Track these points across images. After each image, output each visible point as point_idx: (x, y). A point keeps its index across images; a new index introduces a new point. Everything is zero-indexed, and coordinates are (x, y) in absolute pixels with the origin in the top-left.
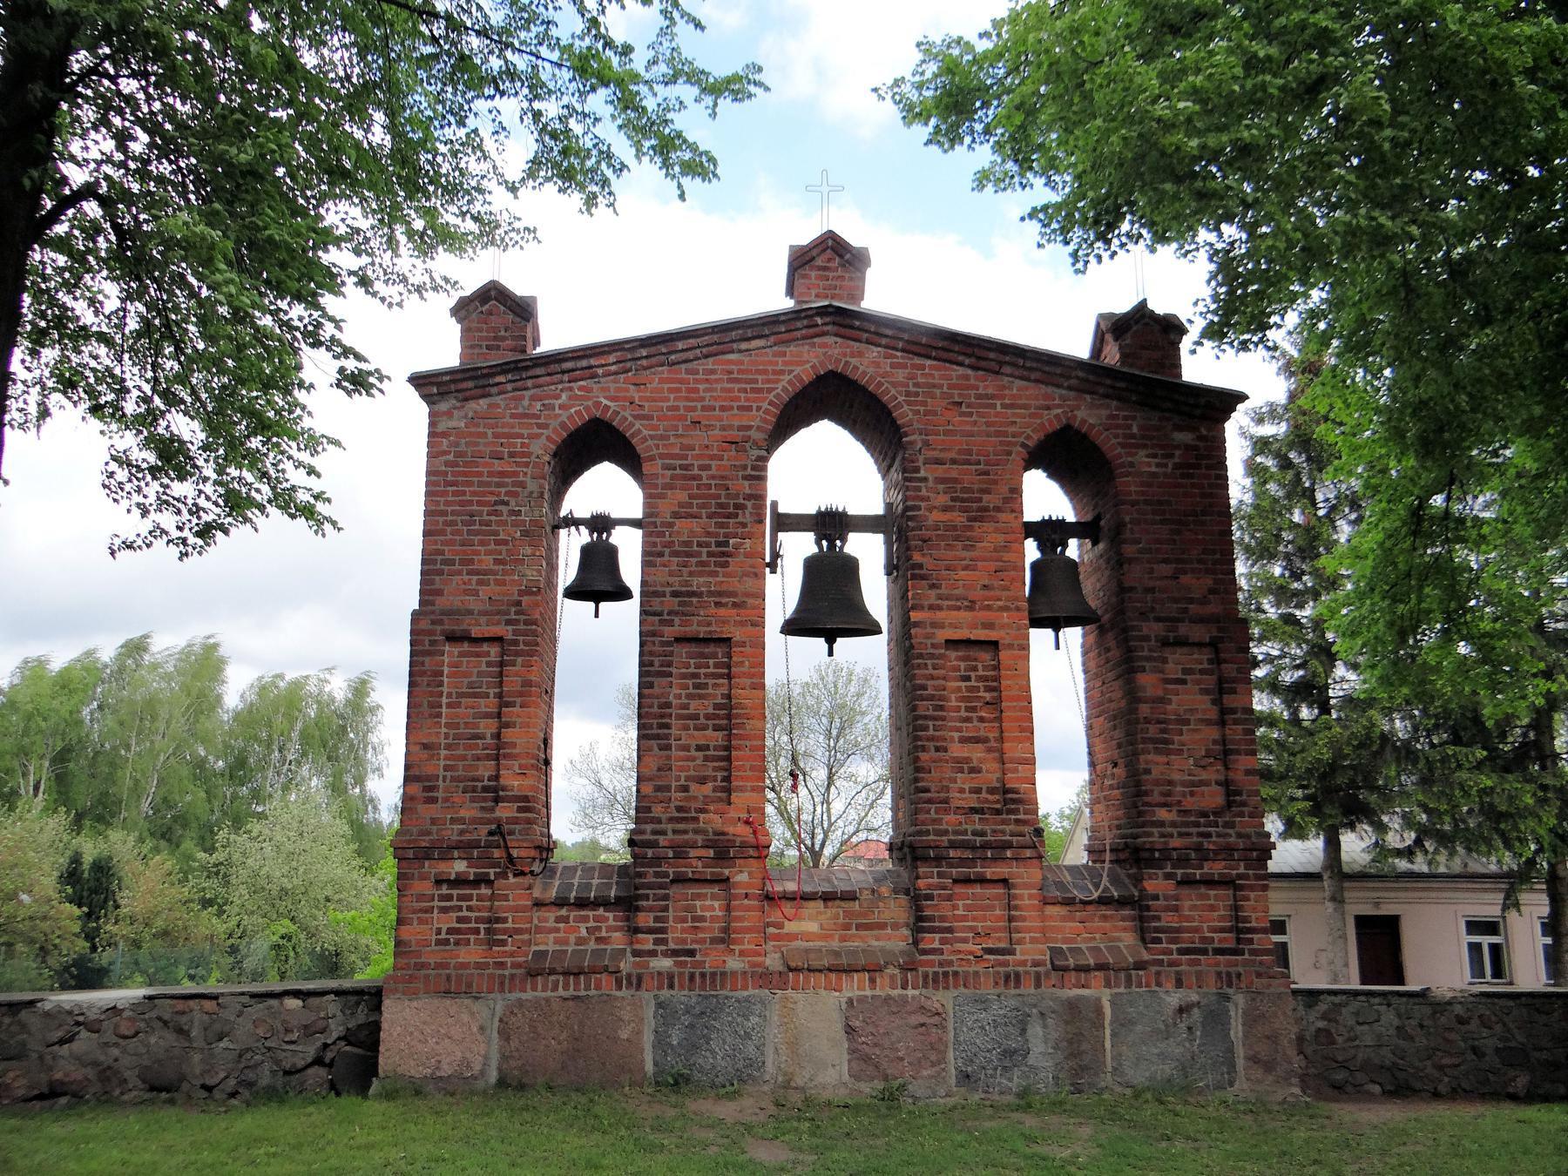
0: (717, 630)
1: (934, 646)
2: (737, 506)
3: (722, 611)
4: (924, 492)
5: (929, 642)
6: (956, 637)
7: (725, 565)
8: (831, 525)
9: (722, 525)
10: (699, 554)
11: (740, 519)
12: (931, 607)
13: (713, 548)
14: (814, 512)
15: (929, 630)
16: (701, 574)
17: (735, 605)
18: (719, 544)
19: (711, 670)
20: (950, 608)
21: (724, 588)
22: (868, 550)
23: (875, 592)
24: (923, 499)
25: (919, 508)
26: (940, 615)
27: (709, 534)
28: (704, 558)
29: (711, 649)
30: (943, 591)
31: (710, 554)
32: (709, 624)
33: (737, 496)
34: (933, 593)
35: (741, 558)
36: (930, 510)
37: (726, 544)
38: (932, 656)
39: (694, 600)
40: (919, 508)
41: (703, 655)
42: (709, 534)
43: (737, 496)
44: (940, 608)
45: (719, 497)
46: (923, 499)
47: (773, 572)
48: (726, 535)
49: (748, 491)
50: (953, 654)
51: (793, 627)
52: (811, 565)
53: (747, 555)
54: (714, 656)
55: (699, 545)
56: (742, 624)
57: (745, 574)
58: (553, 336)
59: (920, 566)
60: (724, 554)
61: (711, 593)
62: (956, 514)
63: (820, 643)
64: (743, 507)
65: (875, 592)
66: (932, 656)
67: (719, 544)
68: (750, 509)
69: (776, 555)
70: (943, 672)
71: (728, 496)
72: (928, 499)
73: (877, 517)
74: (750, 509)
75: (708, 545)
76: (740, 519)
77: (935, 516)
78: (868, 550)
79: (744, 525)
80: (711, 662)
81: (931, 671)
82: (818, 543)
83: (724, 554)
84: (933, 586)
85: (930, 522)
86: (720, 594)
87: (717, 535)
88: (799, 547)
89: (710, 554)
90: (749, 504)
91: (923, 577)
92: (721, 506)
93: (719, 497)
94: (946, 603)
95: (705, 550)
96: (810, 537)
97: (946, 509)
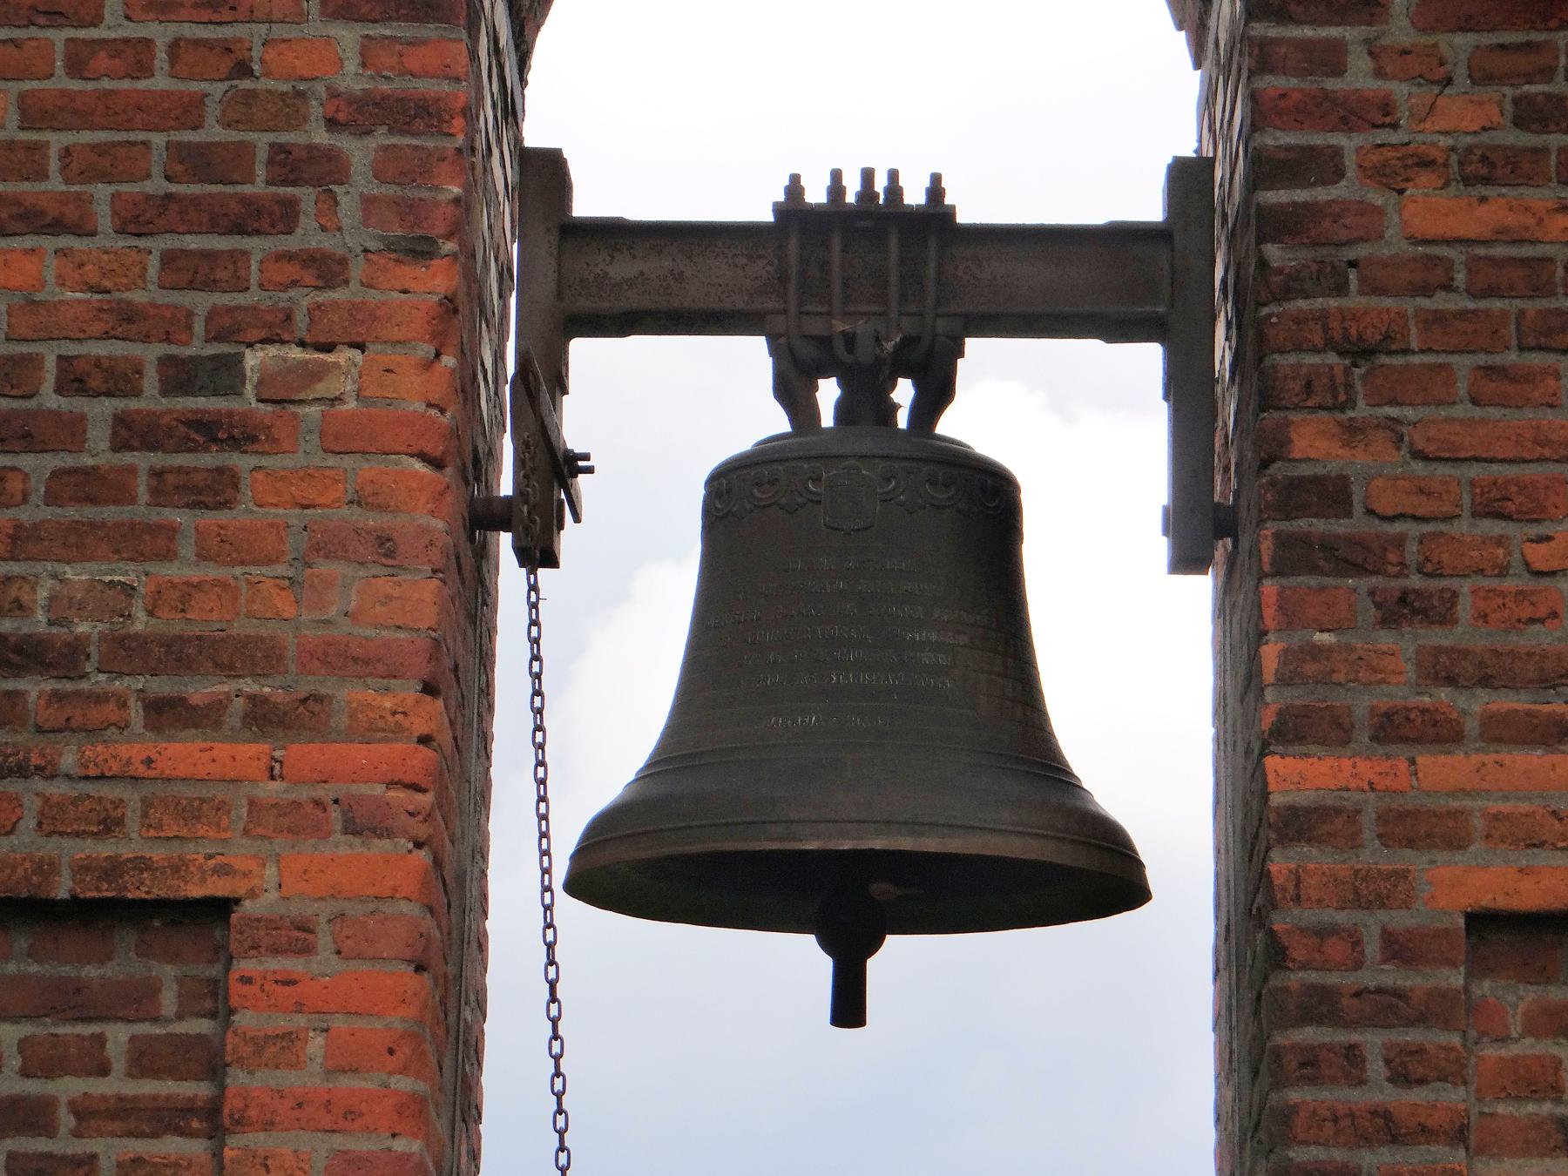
0: (152, 858)
1: (1399, 949)
2: (291, 165)
3: (184, 753)
4: (1359, 77)
5: (1371, 924)
6: (1530, 896)
7: (216, 491)
8: (871, 286)
9: (188, 271)
10: (72, 431)
11: (308, 236)
12: (1393, 729)
13: (151, 400)
14: (1199, 592)
15: (1374, 857)
16: (77, 543)
17: (263, 718)
18: (180, 376)
19: (116, 1085)
20: (1500, 731)
21: (204, 618)
22: (1076, 437)
23: (1130, 671)
24: (1350, 113)
25: (1327, 166)
26: (1440, 772)
27: (128, 320)
28: (98, 452)
29: (118, 963)
30: (1464, 634)
31: (128, 433)
32: (109, 825)
33: (291, 107)
34: (1403, 646)
35: (306, 455)
36: (1392, 173)
37: (225, 374)
38: (1388, 1007)
39: (34, 688)
40: (1327, 166)
41: (73, 1002)
42: (128, 320)
43: (291, 107)
44: (1441, 732)
45: (189, 112)
46: (1350, 113)
47: (539, 554)
48: (225, 328)
49: (352, 79)
50: (1515, 998)
51: (646, 864)
52: (742, 502)
53: (337, 441)
54: (135, 1001)
55: (73, 380)
56: (297, 820)
57: (326, 546)
58: (584, 205)
59: (1332, 495)
60: (208, 431)
61: (127, 652)
62: (1541, 197)
63: (799, 961)
64: (323, 170)
65: (1130, 671)
66: (1388, 1007)
67: (180, 376)
68: (361, 180)
69: (553, 469)
70: (1454, 1096)
71: (243, 110)
72: (1384, 113)
73: (1120, 238)
74: (361, 180)
75: (120, 381)
76: (308, 236)
77: (1429, 211)
78: (1076, 437)
79: (328, 270)
80: (118, 1036)
81: (1379, 1093)
82: (793, 390)
83: (208, 431)
84: (1401, 610)
85: (1393, 244)
86: (177, 654)
87: (174, 325)
88: (669, 416)
89: (128, 433)
90: (359, 152)
91: (1351, 559)
92: (196, 162)
93: (189, 112)
94: (1475, 704)
95: (100, 411)
96: (746, 359)
97: (1484, 169)
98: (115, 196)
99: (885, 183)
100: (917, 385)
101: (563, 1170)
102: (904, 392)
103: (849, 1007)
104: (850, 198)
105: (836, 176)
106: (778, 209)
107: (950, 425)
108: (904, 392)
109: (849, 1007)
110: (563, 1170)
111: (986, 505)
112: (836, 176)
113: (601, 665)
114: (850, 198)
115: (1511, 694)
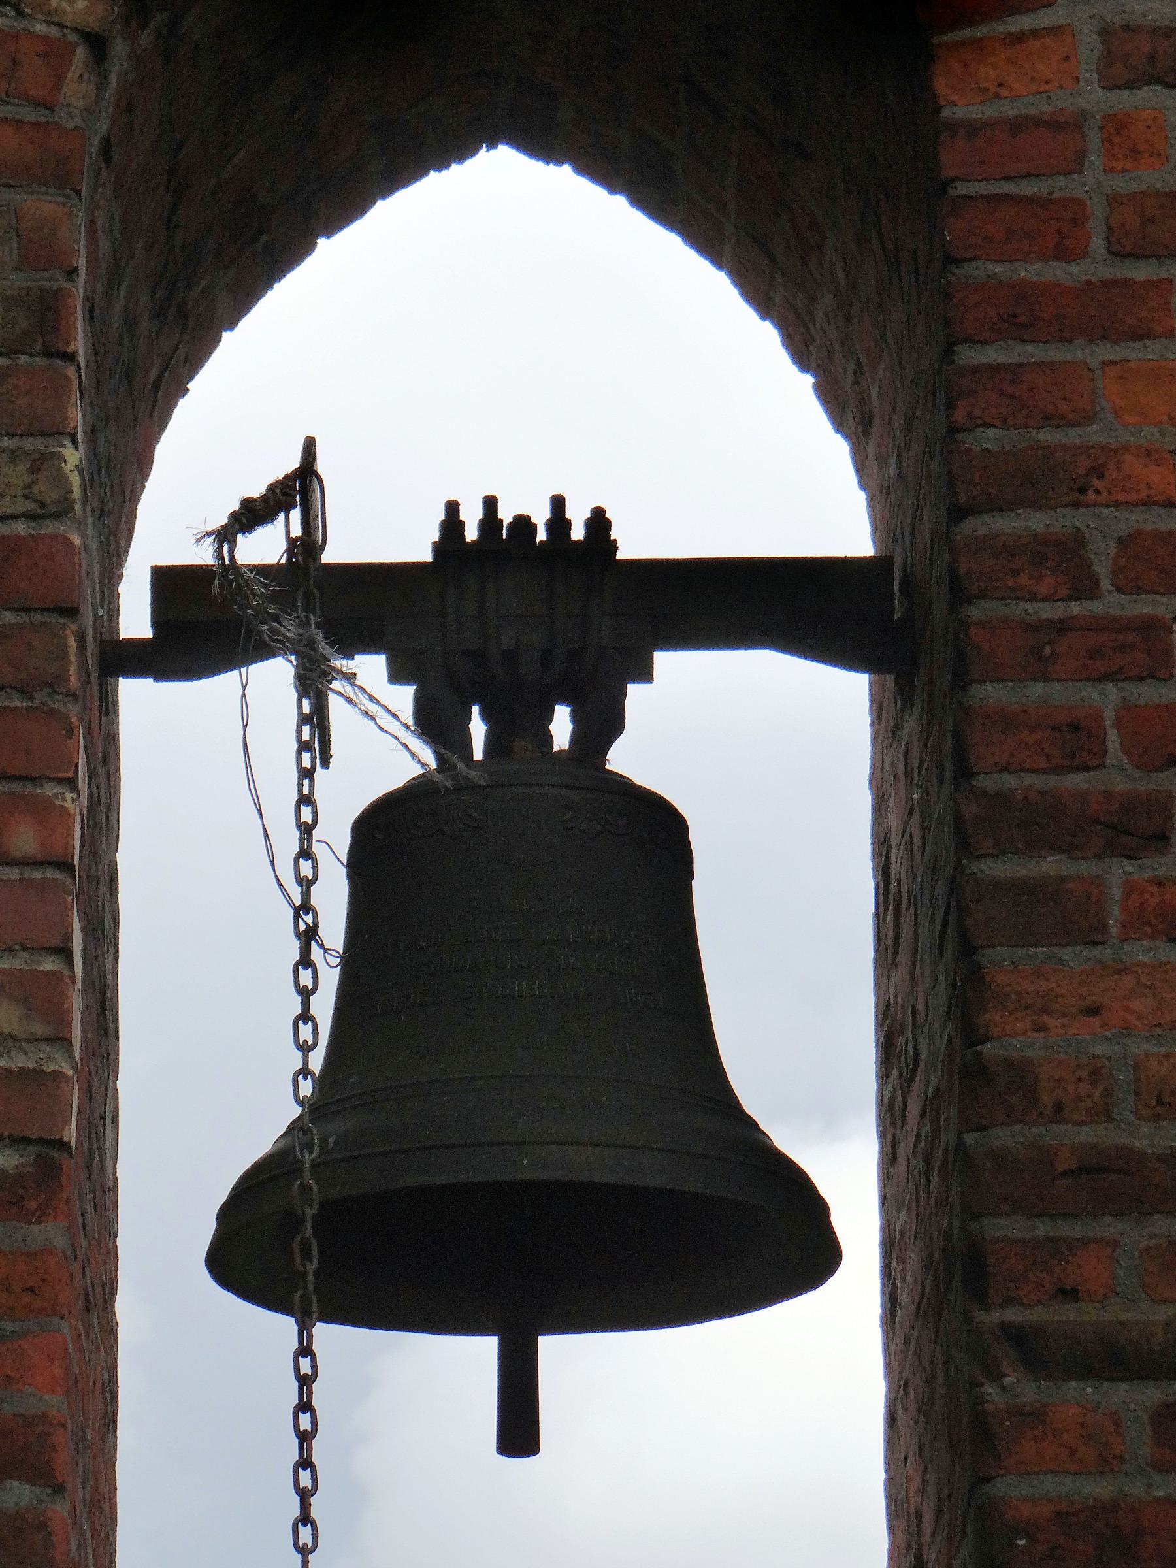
51: (308, 1241)
82: (437, 723)
98: (1127, 706)
99: (479, 515)
100: (575, 717)
101: (305, 1552)
102: (562, 727)
103: (518, 1431)
104: (471, 534)
105: (452, 508)
106: (437, 548)
107: (623, 758)
108: (562, 727)
109: (518, 1431)
110: (305, 1552)
111: (656, 836)
112: (452, 508)
113: (215, 1024)
114: (471, 534)
115: (1108, 345)
